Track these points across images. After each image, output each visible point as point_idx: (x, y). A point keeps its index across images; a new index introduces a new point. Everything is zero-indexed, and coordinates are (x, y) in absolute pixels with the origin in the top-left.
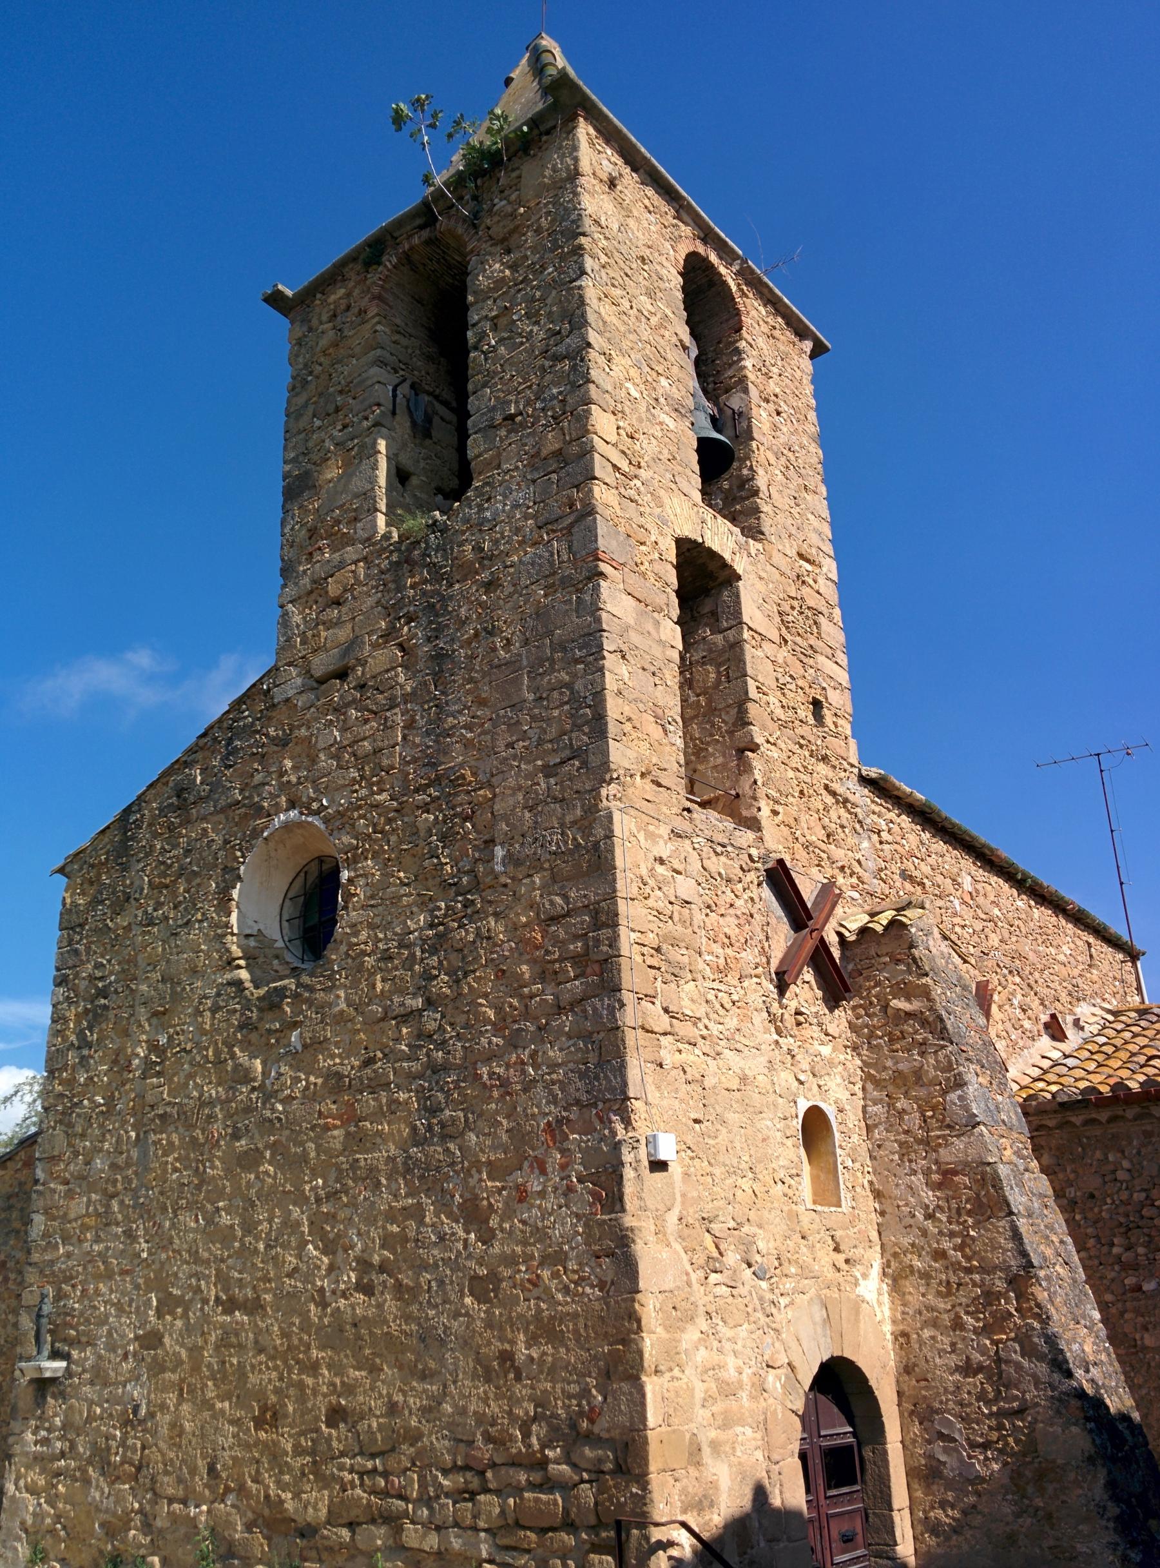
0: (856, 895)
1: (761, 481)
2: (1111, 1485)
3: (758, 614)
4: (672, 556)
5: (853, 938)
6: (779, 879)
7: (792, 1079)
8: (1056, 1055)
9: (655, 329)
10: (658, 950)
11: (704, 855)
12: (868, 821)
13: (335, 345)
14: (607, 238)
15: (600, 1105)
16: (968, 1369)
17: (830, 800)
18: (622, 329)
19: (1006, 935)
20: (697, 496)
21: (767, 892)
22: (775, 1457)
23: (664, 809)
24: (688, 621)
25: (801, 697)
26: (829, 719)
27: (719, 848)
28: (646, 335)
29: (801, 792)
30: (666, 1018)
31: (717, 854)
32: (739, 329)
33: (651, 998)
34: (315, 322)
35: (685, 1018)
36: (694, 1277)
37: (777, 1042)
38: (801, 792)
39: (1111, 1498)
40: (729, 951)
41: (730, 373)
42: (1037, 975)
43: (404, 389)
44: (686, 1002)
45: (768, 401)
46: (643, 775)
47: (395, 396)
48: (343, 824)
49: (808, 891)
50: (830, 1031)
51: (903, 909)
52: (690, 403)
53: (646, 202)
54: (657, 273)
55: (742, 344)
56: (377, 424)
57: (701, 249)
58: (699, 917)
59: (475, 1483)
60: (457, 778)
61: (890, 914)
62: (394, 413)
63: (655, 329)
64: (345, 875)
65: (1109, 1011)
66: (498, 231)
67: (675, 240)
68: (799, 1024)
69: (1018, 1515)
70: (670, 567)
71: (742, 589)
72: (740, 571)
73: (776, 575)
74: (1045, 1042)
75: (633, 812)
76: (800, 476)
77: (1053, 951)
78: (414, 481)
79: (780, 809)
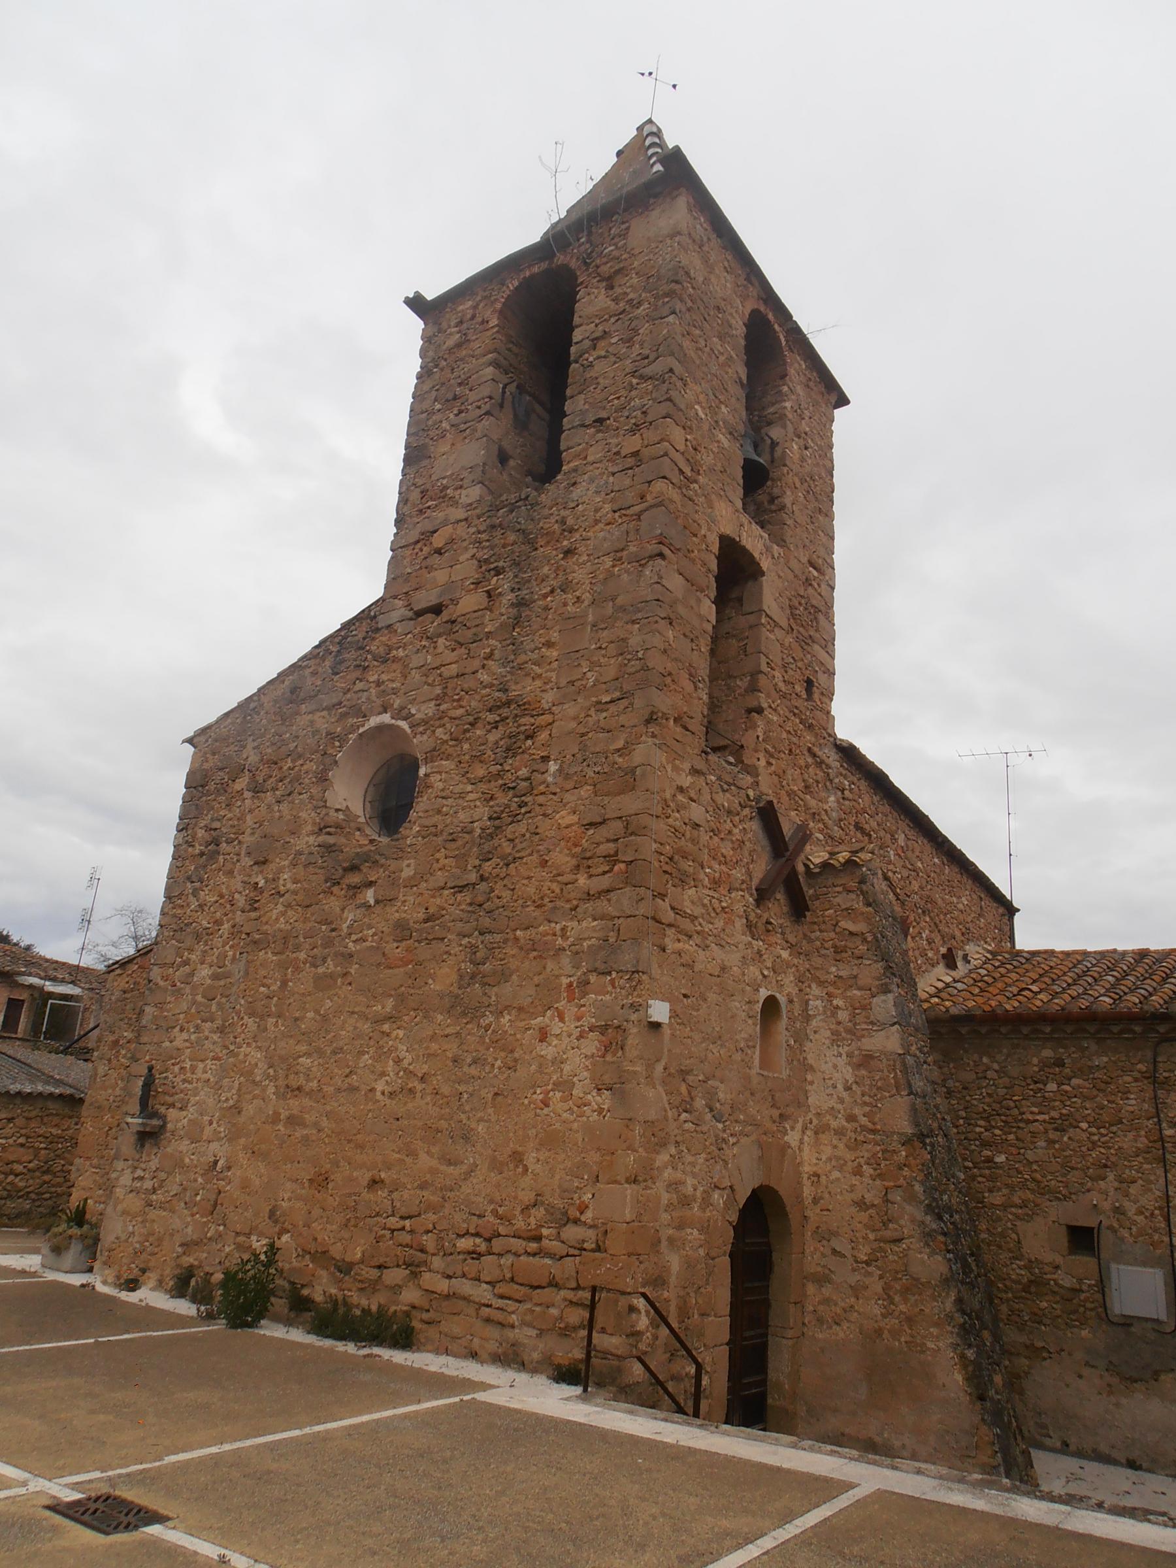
0: (821, 837)
1: (788, 500)
2: (959, 1301)
3: (774, 605)
4: (715, 548)
5: (817, 870)
6: (768, 816)
7: (757, 973)
8: (948, 979)
9: (721, 366)
10: (671, 859)
11: (714, 789)
12: (837, 780)
13: (459, 345)
14: (693, 288)
15: (614, 974)
16: (861, 1204)
17: (810, 760)
18: (698, 362)
19: (924, 883)
20: (739, 504)
21: (755, 826)
22: (713, 1254)
23: (688, 749)
24: (721, 601)
25: (798, 675)
26: (816, 696)
27: (728, 786)
28: (714, 369)
29: (790, 750)
30: (671, 914)
31: (724, 791)
32: (783, 376)
33: (662, 896)
34: (444, 325)
35: (685, 915)
36: (670, 1114)
37: (750, 943)
38: (790, 750)
39: (958, 1311)
40: (723, 867)
41: (771, 410)
42: (942, 917)
43: (512, 388)
44: (687, 903)
45: (799, 437)
46: (675, 720)
47: (504, 392)
48: (426, 730)
49: (787, 829)
50: (790, 939)
51: (857, 852)
52: (741, 428)
53: (726, 264)
54: (728, 321)
55: (785, 388)
56: (487, 413)
57: (762, 309)
58: (705, 838)
59: (483, 1247)
60: (524, 704)
61: (846, 855)
62: (501, 406)
63: (721, 366)
64: (422, 771)
65: (989, 951)
66: (605, 270)
67: (744, 298)
68: (768, 931)
69: (884, 1316)
70: (713, 557)
71: (765, 584)
72: (765, 569)
73: (791, 576)
74: (940, 970)
75: (664, 748)
76: (817, 499)
77: (955, 900)
78: (512, 463)
79: (773, 761)
